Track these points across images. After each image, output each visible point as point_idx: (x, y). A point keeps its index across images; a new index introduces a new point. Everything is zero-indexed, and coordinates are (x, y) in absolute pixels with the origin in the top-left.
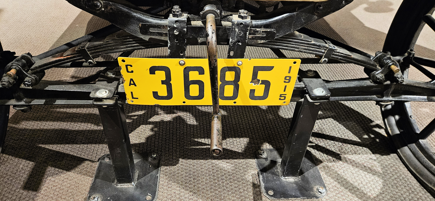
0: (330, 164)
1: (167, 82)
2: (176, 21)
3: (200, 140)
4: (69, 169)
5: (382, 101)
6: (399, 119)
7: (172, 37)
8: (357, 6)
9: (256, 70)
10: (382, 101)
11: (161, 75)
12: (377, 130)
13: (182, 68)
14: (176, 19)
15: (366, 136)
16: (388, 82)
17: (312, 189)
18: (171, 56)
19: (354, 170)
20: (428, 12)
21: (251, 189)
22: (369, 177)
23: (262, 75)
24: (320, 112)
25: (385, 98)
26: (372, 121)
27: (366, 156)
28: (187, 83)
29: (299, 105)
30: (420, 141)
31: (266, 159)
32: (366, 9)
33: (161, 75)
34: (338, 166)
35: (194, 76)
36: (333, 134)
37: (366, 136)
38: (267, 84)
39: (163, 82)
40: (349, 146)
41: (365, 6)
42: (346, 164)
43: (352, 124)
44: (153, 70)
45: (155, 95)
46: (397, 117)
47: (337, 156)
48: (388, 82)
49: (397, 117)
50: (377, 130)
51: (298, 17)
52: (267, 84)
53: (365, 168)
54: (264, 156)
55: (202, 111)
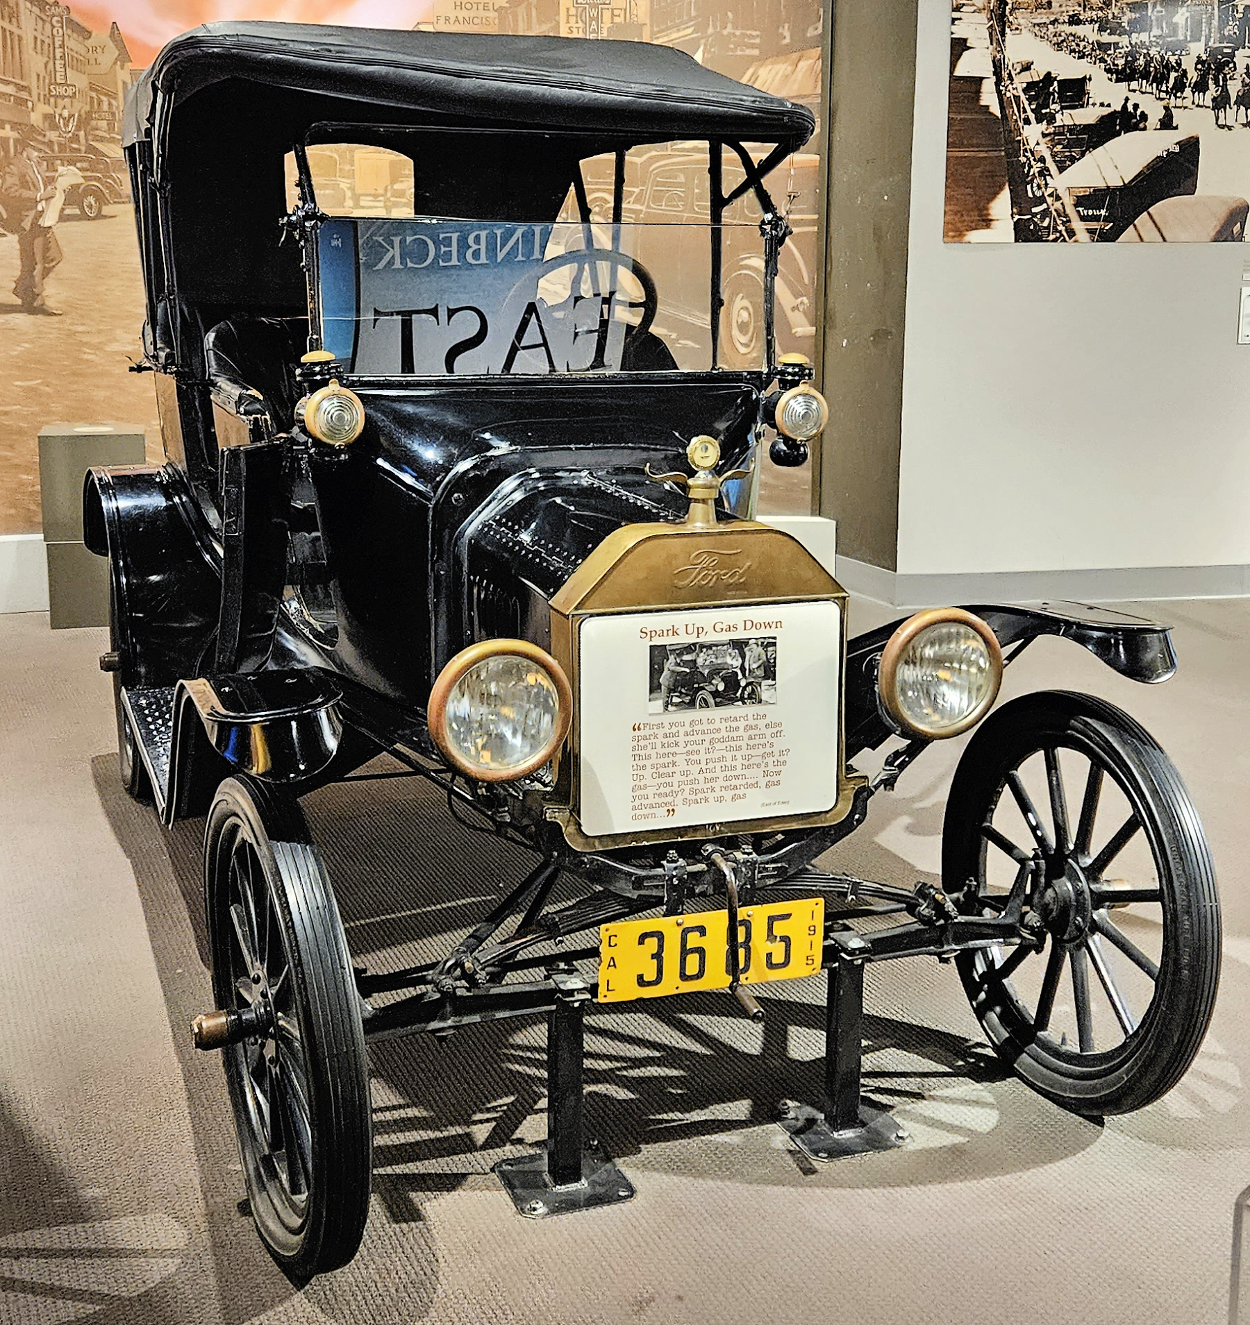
0: (908, 1108)
1: (658, 956)
2: (675, 868)
3: (665, 1116)
4: (454, 1188)
5: (944, 953)
6: (1002, 1012)
7: (673, 888)
8: (882, 826)
9: (772, 920)
10: (944, 953)
11: (652, 943)
12: (979, 1050)
13: (680, 929)
14: (674, 865)
15: (961, 1063)
16: (942, 922)
17: (888, 1139)
18: (668, 914)
19: (950, 1108)
20: (984, 820)
21: (788, 1157)
22: (977, 1111)
23: (780, 928)
24: (864, 1043)
25: (946, 948)
26: (967, 1041)
27: (966, 1087)
28: (685, 952)
29: (833, 974)
30: (1040, 1034)
31: (796, 1119)
32: (911, 829)
33: (652, 943)
34: (920, 1107)
35: (694, 940)
36: (901, 1069)
37: (961, 1063)
38: (786, 940)
39: (653, 956)
40: (934, 1079)
41: (906, 820)
42: (933, 1103)
43: (930, 1050)
44: (642, 938)
45: (641, 982)
46: (998, 1009)
47: (918, 1096)
48: (942, 922)
49: (998, 1009)
50: (979, 1050)
51: (807, 845)
52: (786, 940)
53: (967, 1102)
54: (791, 1115)
55: (634, 1078)
